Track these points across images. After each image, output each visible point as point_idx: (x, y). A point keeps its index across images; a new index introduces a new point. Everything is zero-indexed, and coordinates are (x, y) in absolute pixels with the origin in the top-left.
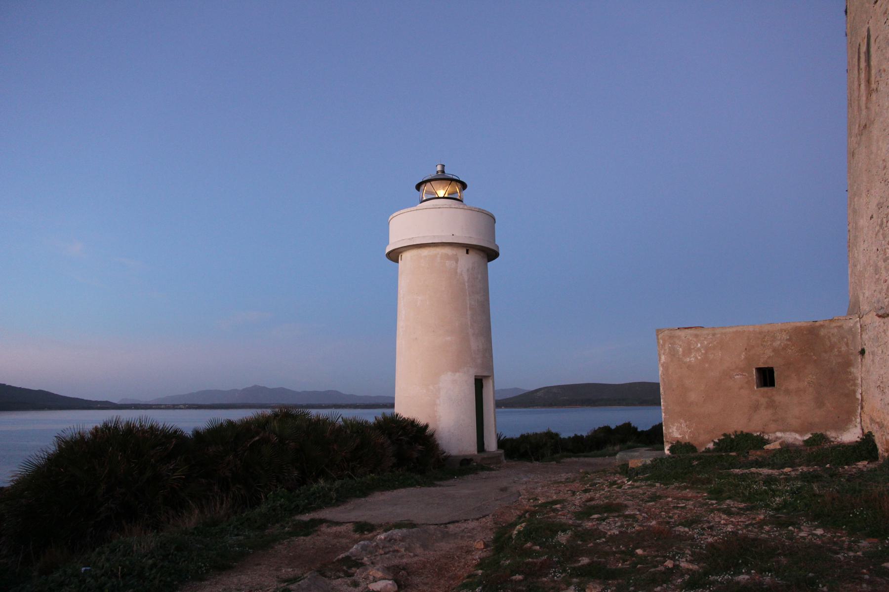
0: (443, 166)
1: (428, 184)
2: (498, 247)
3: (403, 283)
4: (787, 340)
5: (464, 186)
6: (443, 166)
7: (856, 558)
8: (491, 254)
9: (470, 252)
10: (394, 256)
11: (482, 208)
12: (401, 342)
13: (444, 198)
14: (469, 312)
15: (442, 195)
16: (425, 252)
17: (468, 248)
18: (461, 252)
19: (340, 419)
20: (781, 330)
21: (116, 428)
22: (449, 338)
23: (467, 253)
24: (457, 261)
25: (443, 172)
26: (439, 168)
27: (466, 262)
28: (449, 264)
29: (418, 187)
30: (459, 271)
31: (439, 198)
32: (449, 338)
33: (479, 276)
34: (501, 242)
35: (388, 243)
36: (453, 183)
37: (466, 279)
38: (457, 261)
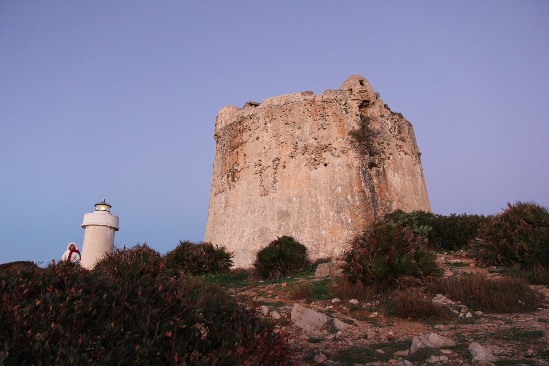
5: (111, 207)
10: (84, 227)
17: (111, 227)
18: (109, 229)
27: (110, 231)
28: (105, 232)
29: (95, 205)
34: (120, 226)
35: (82, 223)
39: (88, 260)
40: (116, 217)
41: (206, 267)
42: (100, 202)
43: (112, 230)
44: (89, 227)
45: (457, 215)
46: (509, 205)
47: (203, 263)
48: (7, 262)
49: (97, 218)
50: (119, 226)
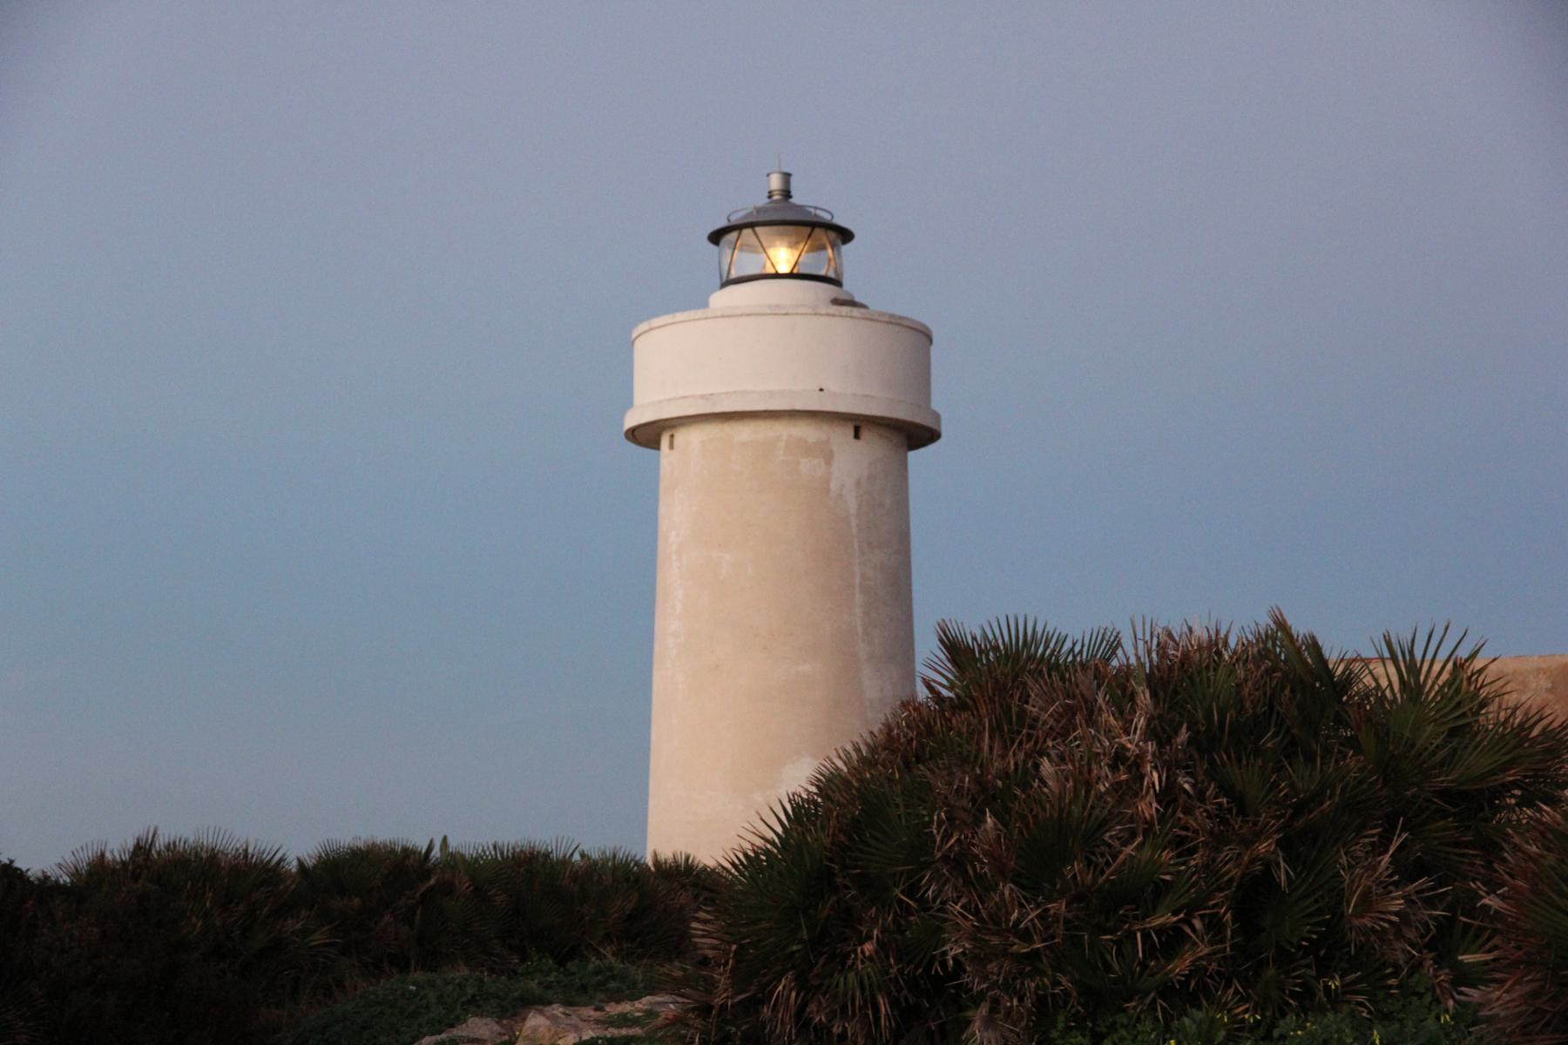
0: (787, 177)
1: (747, 232)
2: (937, 417)
3: (678, 517)
4: (1548, 690)
5: (845, 235)
6: (787, 177)
7: (1158, 755)
8: (917, 435)
9: (865, 434)
10: (648, 436)
11: (898, 312)
12: (671, 676)
13: (791, 276)
14: (859, 598)
15: (784, 268)
16: (744, 432)
17: (859, 424)
18: (841, 437)
19: (577, 857)
20: (1539, 670)
21: (1348, 680)
22: (806, 668)
23: (857, 436)
24: (829, 457)
25: (787, 194)
26: (775, 183)
27: (852, 460)
28: (810, 467)
29: (716, 237)
30: (834, 486)
31: (777, 276)
32: (806, 668)
33: (888, 502)
34: (947, 402)
35: (629, 404)
36: (818, 231)
37: (853, 506)
38: (829, 457)
39: (711, 766)
40: (896, 321)
41: (1173, 940)
42: (752, 197)
43: (872, 448)
44: (684, 436)
45: (160, 843)
46: (687, 858)
47: (1141, 892)
48: (291, 819)
49: (726, 345)
50: (936, 404)
